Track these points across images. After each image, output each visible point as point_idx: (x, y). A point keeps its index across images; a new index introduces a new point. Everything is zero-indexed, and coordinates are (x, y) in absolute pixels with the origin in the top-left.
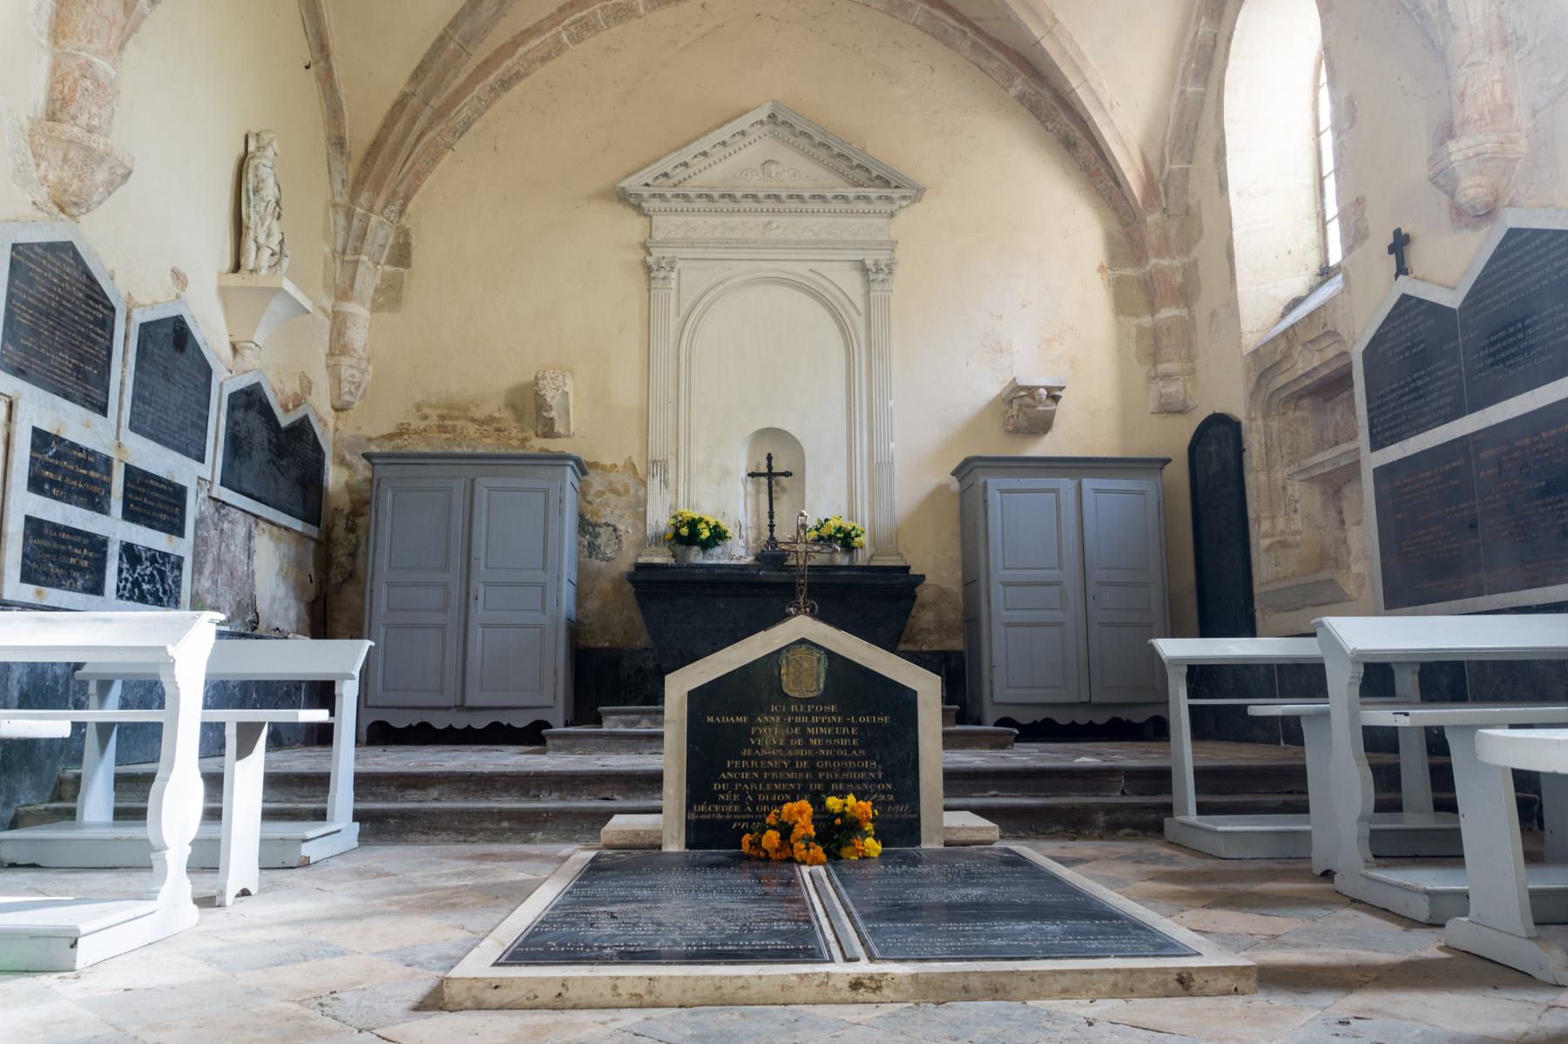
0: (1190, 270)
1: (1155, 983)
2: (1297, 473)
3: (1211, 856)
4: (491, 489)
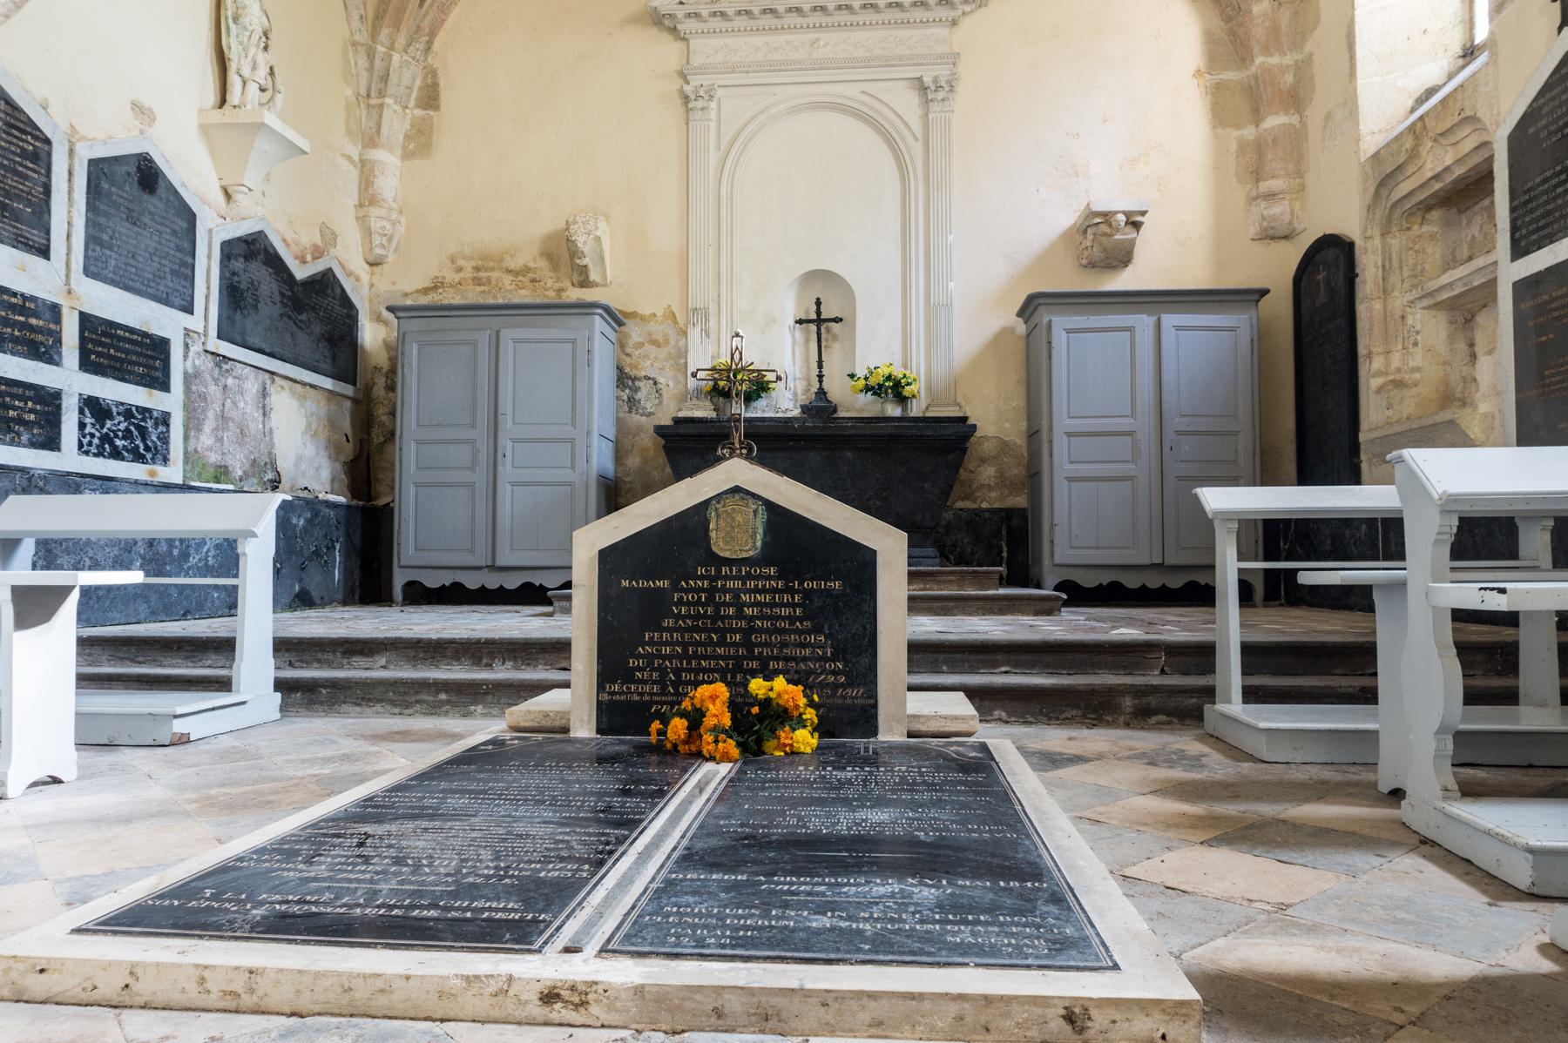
0: (1303, 70)
1: (1027, 1019)
2: (1420, 298)
3: (1252, 758)
4: (516, 341)
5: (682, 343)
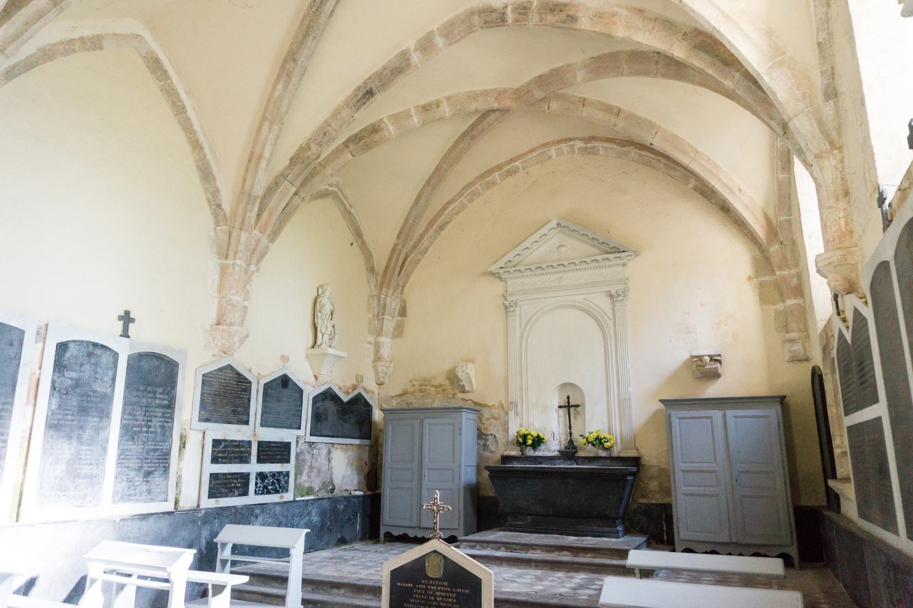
4: (430, 424)
5: (506, 419)
